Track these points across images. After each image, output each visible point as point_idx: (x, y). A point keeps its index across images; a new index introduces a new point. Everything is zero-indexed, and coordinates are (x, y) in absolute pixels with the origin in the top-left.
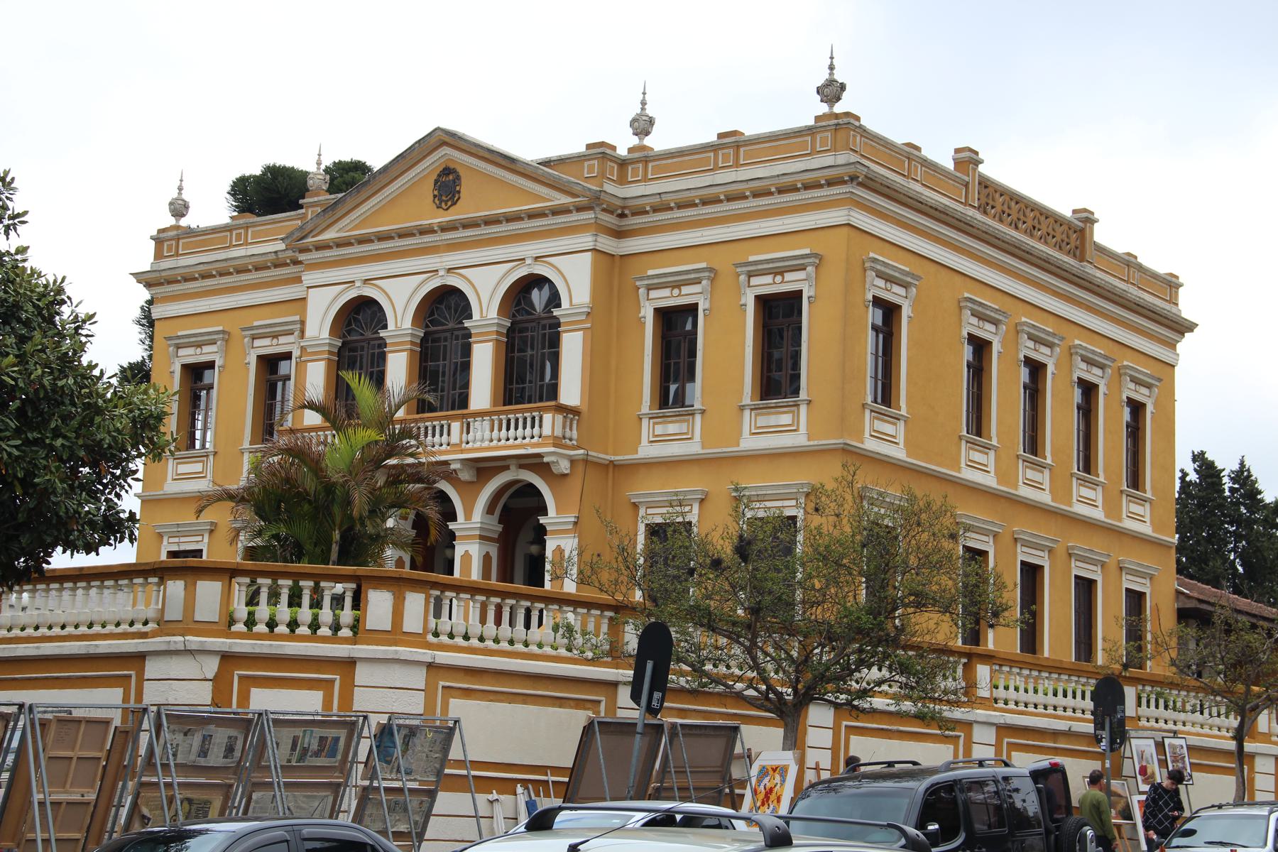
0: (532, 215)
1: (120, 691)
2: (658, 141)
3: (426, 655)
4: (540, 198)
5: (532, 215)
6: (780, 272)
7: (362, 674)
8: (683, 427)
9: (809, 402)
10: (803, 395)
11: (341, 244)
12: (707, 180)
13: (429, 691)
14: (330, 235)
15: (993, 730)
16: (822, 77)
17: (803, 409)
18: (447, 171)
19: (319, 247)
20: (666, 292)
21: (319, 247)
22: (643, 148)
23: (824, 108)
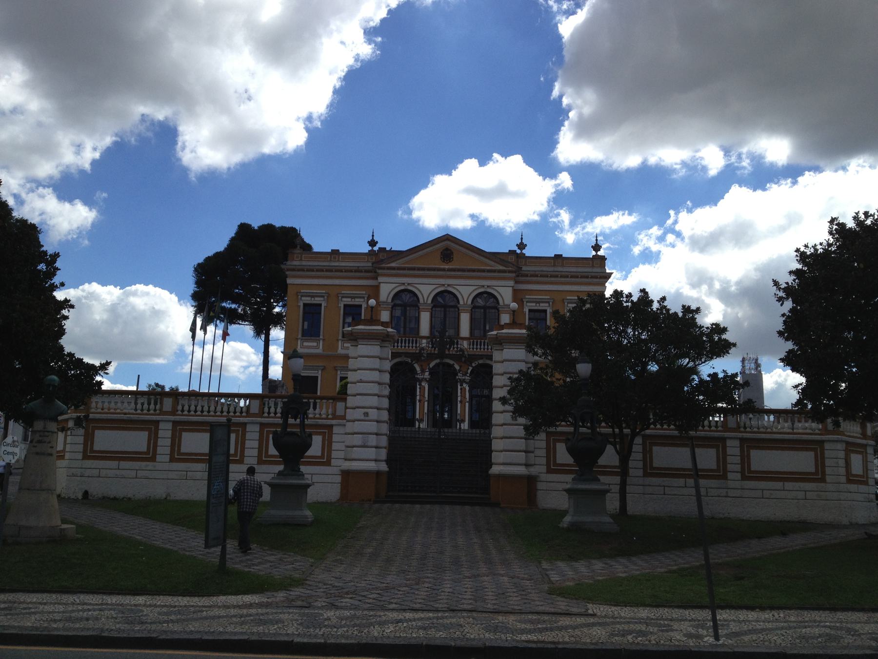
0: (489, 271)
1: (144, 435)
2: (528, 252)
3: (740, 435)
4: (489, 265)
5: (489, 271)
6: (354, 298)
7: (827, 446)
8: (315, 344)
9: (324, 340)
11: (399, 269)
12: (551, 269)
13: (742, 447)
14: (393, 265)
15: (258, 426)
16: (370, 239)
17: (321, 342)
19: (389, 268)
20: (309, 298)
21: (389, 268)
22: (597, 255)
23: (370, 248)
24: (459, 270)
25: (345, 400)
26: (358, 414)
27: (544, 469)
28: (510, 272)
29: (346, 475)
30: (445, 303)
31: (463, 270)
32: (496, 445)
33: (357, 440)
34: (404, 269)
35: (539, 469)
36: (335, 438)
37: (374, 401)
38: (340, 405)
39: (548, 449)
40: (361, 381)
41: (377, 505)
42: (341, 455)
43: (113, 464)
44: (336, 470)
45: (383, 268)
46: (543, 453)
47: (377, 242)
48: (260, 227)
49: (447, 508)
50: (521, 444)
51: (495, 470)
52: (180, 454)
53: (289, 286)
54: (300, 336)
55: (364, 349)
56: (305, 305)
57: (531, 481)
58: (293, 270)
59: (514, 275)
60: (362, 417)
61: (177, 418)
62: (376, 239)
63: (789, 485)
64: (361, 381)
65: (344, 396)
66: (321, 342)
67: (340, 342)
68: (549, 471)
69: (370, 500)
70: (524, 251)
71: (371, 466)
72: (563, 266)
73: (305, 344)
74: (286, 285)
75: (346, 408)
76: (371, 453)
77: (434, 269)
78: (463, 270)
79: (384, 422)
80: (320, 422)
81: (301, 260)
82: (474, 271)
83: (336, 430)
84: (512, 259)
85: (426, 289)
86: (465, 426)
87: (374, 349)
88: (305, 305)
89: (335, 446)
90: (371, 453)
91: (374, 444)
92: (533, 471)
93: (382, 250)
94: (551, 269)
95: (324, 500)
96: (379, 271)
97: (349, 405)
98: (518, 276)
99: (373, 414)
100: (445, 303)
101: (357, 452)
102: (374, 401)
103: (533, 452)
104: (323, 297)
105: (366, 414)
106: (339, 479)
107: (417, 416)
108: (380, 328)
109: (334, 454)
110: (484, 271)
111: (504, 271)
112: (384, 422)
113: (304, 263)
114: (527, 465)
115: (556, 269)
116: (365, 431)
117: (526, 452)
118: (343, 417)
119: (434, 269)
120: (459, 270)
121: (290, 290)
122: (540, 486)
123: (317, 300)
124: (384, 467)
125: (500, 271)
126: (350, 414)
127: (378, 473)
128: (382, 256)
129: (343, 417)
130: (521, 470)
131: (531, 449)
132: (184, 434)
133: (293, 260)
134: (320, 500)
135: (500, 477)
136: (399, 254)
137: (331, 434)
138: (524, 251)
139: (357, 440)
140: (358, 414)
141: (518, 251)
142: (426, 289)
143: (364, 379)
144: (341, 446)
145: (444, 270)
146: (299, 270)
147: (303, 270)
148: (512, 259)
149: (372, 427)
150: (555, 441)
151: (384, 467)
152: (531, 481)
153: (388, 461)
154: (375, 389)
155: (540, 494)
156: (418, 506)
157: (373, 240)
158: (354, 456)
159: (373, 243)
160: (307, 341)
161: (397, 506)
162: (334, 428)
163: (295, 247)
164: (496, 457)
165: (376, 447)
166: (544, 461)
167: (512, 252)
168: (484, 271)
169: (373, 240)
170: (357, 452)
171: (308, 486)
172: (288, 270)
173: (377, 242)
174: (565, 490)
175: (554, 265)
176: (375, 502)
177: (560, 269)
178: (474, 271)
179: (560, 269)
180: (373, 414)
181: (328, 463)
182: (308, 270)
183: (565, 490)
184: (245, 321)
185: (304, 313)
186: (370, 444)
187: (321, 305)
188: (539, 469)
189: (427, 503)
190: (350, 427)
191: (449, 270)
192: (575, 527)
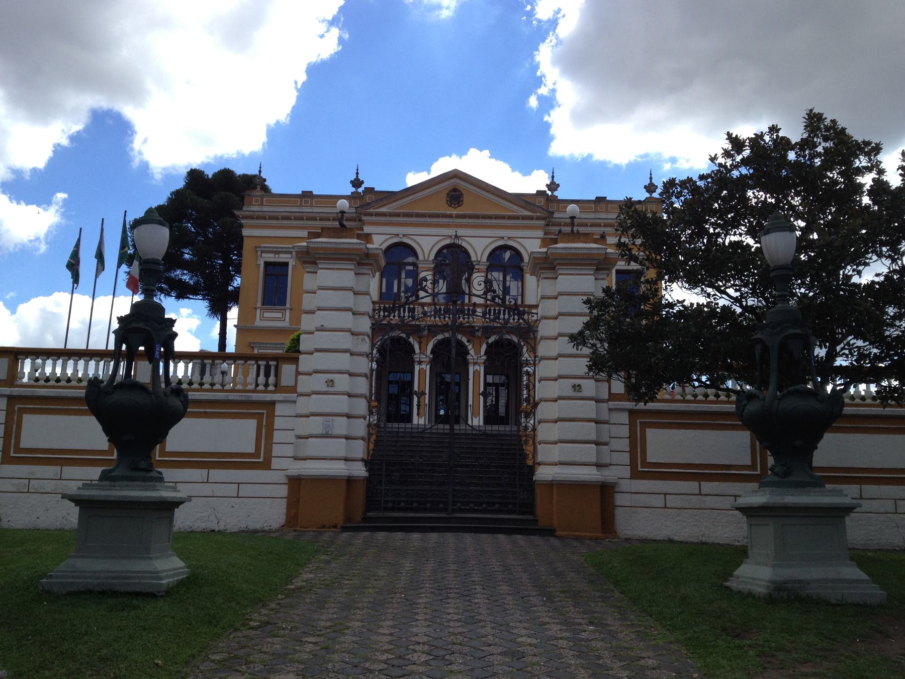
0: (510, 218)
2: (561, 194)
5: (510, 218)
8: (280, 315)
9: (291, 309)
10: (288, 305)
11: (391, 215)
12: (593, 216)
14: (384, 210)
16: (353, 177)
17: (288, 312)
18: (455, 190)
19: (378, 214)
20: (272, 255)
21: (378, 214)
23: (354, 190)
24: (471, 217)
25: (296, 360)
26: (317, 382)
27: (626, 472)
28: (538, 218)
29: (296, 483)
30: (453, 261)
31: (477, 217)
32: (545, 432)
33: (315, 425)
34: (397, 215)
35: (618, 473)
36: (278, 423)
37: (343, 361)
38: (287, 370)
39: (632, 438)
40: (322, 329)
41: (346, 535)
42: (289, 451)
43: (51, 471)
44: (280, 477)
45: (371, 215)
46: (624, 444)
47: (362, 182)
48: (215, 175)
49: (468, 538)
50: (589, 431)
51: (543, 473)
52: (18, 449)
53: (246, 241)
54: (259, 305)
55: (327, 276)
56: (267, 264)
57: (606, 492)
58: (251, 218)
59: (543, 222)
60: (325, 388)
61: (16, 391)
62: (361, 177)
63: (217, 474)
64: (322, 329)
65: (294, 355)
66: (288, 312)
67: (258, 311)
68: (636, 475)
69: (335, 527)
70: (555, 193)
71: (339, 469)
72: (607, 212)
73: (266, 315)
74: (241, 238)
75: (298, 373)
76: (338, 447)
77: (437, 216)
78: (477, 217)
79: (360, 396)
80: (255, 397)
81: (262, 205)
82: (490, 217)
83: (279, 409)
84: (542, 201)
85: (427, 243)
86: (477, 421)
87: (344, 276)
88: (267, 264)
89: (277, 436)
90: (338, 447)
91: (344, 432)
92: (609, 475)
93: (370, 190)
94: (593, 216)
95: (258, 526)
96: (364, 218)
97: (301, 369)
98: (548, 225)
99: (343, 382)
100: (453, 261)
101: (315, 447)
102: (343, 361)
103: (606, 444)
104: (291, 253)
105: (331, 383)
106: (284, 491)
107: (416, 388)
108: (355, 241)
109: (276, 450)
110: (503, 217)
111: (531, 218)
112: (360, 396)
113: (266, 209)
114: (599, 466)
115: (598, 216)
116: (328, 410)
117: (597, 444)
118: (293, 389)
119: (437, 216)
120: (471, 217)
121: (247, 246)
122: (620, 499)
123: (283, 258)
124: (359, 470)
125: (525, 218)
126: (305, 383)
127: (350, 481)
128: (368, 199)
129: (293, 389)
130: (589, 474)
131: (606, 439)
132: (26, 417)
133: (252, 204)
134: (252, 526)
135: (551, 485)
136: (389, 196)
137: (271, 416)
138: (555, 193)
139: (315, 425)
140: (317, 382)
141: (549, 193)
142: (427, 243)
143: (327, 325)
144: (290, 437)
145: (450, 216)
146: (258, 218)
147: (264, 218)
148: (542, 201)
149: (341, 404)
150: (644, 426)
151: (359, 470)
152: (606, 492)
153: (368, 463)
154: (346, 341)
155: (620, 516)
156: (416, 536)
157: (357, 179)
158: (310, 453)
159: (357, 183)
160: (268, 310)
161: (381, 536)
162: (277, 406)
163: (255, 188)
164: (544, 453)
165: (347, 438)
166: (626, 458)
167: (540, 193)
168: (503, 217)
169: (357, 179)
170: (315, 447)
171: (177, 504)
172: (244, 217)
173: (362, 182)
174: (742, 509)
175: (596, 211)
176: (345, 529)
177: (603, 216)
178: (490, 217)
179: (603, 216)
180: (343, 382)
181: (266, 465)
182: (271, 218)
183: (742, 509)
184: (197, 294)
185: (266, 275)
186: (336, 432)
187: (287, 264)
188: (618, 473)
189: (433, 530)
190: (304, 405)
191: (458, 216)
192: (784, 596)
